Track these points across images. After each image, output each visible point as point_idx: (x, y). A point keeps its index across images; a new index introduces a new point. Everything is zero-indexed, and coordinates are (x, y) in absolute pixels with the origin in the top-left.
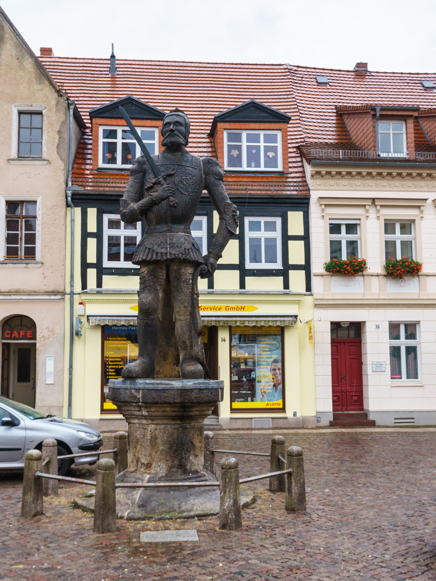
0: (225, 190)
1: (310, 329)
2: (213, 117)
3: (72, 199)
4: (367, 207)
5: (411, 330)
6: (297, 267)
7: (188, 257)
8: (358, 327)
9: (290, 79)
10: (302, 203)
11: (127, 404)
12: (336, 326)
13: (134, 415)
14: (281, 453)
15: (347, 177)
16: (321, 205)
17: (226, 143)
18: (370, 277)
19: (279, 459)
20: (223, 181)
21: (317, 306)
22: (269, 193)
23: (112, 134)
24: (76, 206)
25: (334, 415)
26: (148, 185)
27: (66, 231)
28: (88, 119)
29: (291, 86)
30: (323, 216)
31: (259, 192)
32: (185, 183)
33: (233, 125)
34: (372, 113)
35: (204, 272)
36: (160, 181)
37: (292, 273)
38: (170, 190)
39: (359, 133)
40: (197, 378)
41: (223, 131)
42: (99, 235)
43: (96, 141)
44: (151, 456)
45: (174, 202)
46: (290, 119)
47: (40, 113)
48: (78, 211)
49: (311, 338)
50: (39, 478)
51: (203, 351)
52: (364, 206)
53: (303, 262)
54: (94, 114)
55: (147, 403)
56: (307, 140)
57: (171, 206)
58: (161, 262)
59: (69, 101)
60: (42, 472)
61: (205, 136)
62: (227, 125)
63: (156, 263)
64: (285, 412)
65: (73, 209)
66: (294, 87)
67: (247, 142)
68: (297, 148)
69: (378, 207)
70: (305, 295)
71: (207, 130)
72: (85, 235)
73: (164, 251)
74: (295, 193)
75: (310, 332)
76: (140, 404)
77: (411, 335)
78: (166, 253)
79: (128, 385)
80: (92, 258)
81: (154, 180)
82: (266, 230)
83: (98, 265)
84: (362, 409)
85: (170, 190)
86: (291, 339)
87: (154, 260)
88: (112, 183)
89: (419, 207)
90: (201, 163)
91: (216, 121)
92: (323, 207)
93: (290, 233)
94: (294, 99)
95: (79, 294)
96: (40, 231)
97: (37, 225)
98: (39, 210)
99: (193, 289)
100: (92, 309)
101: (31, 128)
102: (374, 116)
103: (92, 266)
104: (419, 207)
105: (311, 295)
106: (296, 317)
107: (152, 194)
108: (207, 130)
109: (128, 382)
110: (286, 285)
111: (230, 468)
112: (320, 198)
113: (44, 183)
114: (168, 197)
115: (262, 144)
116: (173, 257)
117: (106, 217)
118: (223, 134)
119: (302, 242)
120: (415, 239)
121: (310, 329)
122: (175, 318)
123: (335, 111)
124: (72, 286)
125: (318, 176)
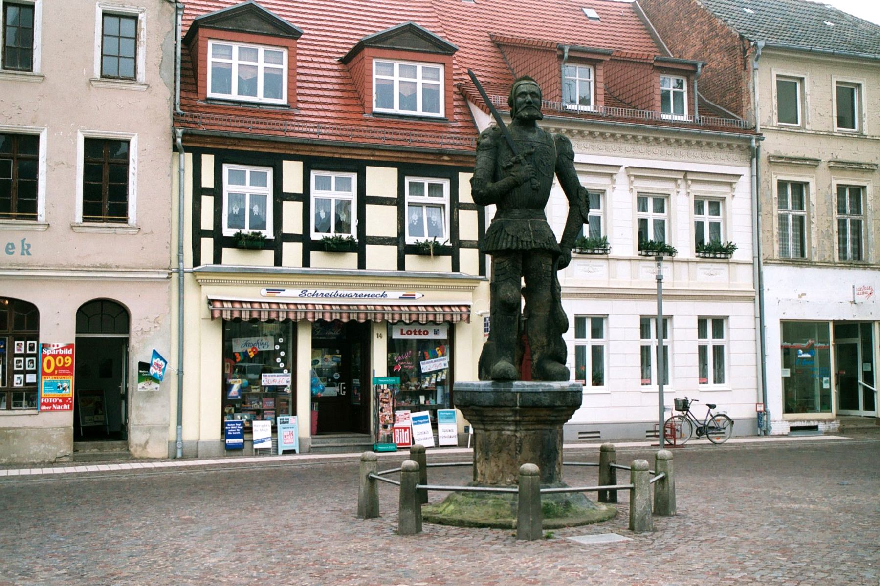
4: (679, 182)
5: (719, 323)
18: (616, 261)
27: (171, 185)
31: (326, 137)
34: (559, 53)
37: (286, 246)
42: (216, 192)
43: (206, 61)
47: (135, 18)
48: (189, 157)
52: (675, 180)
57: (533, 189)
61: (334, 61)
65: (182, 156)
69: (690, 182)
72: (199, 191)
74: (461, 148)
77: (597, 332)
79: (502, 387)
80: (207, 223)
82: (337, 189)
89: (611, 175)
92: (632, 178)
93: (369, 193)
94: (436, 19)
101: (119, 37)
102: (561, 57)
103: (207, 234)
104: (731, 184)
120: (725, 220)
123: (489, 39)
124: (180, 260)
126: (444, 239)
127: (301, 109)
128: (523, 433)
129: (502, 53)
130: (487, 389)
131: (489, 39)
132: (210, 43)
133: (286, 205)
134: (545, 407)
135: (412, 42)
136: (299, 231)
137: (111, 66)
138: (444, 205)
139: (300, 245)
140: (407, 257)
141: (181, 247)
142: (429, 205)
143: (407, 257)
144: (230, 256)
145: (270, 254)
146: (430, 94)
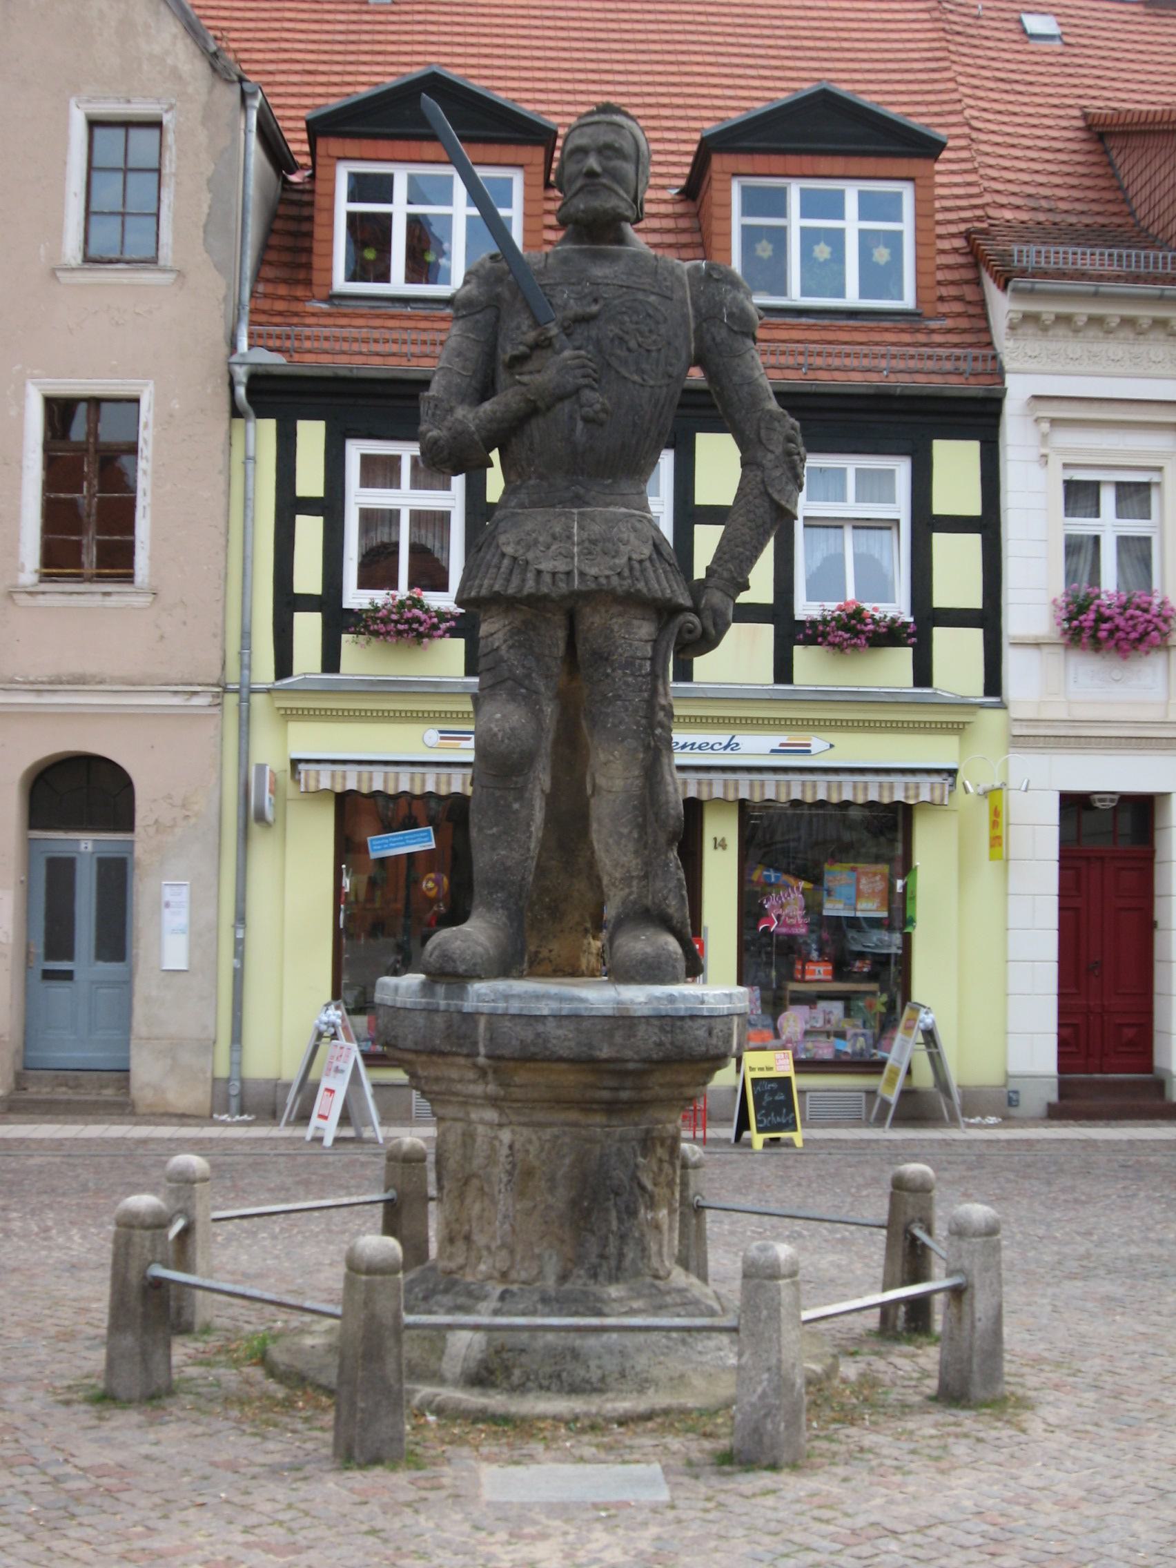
0: (768, 368)
1: (996, 813)
2: (697, 136)
3: (249, 392)
7: (641, 585)
8: (1142, 811)
9: (937, 20)
10: (978, 417)
11: (435, 1058)
12: (1074, 805)
13: (456, 1094)
14: (921, 1220)
15: (1121, 334)
16: (1037, 420)
17: (737, 221)
19: (914, 1239)
20: (755, 340)
21: (1018, 741)
22: (874, 377)
23: (380, 188)
24: (260, 414)
26: (508, 351)
28: (302, 141)
29: (944, 44)
30: (1044, 456)
32: (633, 344)
33: (761, 162)
36: (550, 339)
37: (942, 636)
38: (584, 366)
39: (1157, 195)
41: (729, 182)
42: (330, 506)
43: (331, 210)
45: (598, 407)
46: (942, 146)
47: (157, 124)
48: (268, 428)
49: (996, 841)
50: (159, 1283)
54: (319, 128)
55: (500, 1058)
56: (992, 212)
58: (553, 601)
59: (246, 86)
60: (167, 1267)
62: (742, 162)
63: (536, 602)
65: (251, 425)
66: (952, 48)
67: (804, 215)
68: (967, 235)
70: (982, 706)
71: (676, 176)
72: (290, 505)
73: (561, 566)
75: (995, 824)
76: (481, 1060)
78: (569, 574)
80: (308, 579)
81: (531, 336)
82: (415, 485)
83: (328, 602)
84: (1148, 1067)
85: (584, 366)
86: (931, 847)
87: (530, 596)
88: (376, 341)
90: (686, 278)
91: (709, 147)
92: (1045, 426)
94: (951, 85)
95: (268, 691)
96: (149, 493)
97: (140, 474)
98: (146, 426)
100: (312, 739)
101: (126, 171)
103: (308, 603)
105: (1002, 706)
106: (952, 773)
107: (525, 379)
108: (676, 176)
110: (923, 675)
112: (1036, 397)
113: (167, 341)
114: (577, 391)
115: (852, 224)
116: (593, 586)
117: (355, 450)
118: (729, 190)
120: (1161, 526)
121: (996, 813)
122: (594, 786)
123: (1080, 124)
124: (246, 665)
125: (1030, 329)
126: (899, 607)
129: (1106, 152)
133: (941, 542)
134: (561, 1059)
135: (829, 130)
137: (106, 235)
138: (897, 522)
139: (768, 629)
141: (246, 636)
142: (862, 525)
144: (356, 656)
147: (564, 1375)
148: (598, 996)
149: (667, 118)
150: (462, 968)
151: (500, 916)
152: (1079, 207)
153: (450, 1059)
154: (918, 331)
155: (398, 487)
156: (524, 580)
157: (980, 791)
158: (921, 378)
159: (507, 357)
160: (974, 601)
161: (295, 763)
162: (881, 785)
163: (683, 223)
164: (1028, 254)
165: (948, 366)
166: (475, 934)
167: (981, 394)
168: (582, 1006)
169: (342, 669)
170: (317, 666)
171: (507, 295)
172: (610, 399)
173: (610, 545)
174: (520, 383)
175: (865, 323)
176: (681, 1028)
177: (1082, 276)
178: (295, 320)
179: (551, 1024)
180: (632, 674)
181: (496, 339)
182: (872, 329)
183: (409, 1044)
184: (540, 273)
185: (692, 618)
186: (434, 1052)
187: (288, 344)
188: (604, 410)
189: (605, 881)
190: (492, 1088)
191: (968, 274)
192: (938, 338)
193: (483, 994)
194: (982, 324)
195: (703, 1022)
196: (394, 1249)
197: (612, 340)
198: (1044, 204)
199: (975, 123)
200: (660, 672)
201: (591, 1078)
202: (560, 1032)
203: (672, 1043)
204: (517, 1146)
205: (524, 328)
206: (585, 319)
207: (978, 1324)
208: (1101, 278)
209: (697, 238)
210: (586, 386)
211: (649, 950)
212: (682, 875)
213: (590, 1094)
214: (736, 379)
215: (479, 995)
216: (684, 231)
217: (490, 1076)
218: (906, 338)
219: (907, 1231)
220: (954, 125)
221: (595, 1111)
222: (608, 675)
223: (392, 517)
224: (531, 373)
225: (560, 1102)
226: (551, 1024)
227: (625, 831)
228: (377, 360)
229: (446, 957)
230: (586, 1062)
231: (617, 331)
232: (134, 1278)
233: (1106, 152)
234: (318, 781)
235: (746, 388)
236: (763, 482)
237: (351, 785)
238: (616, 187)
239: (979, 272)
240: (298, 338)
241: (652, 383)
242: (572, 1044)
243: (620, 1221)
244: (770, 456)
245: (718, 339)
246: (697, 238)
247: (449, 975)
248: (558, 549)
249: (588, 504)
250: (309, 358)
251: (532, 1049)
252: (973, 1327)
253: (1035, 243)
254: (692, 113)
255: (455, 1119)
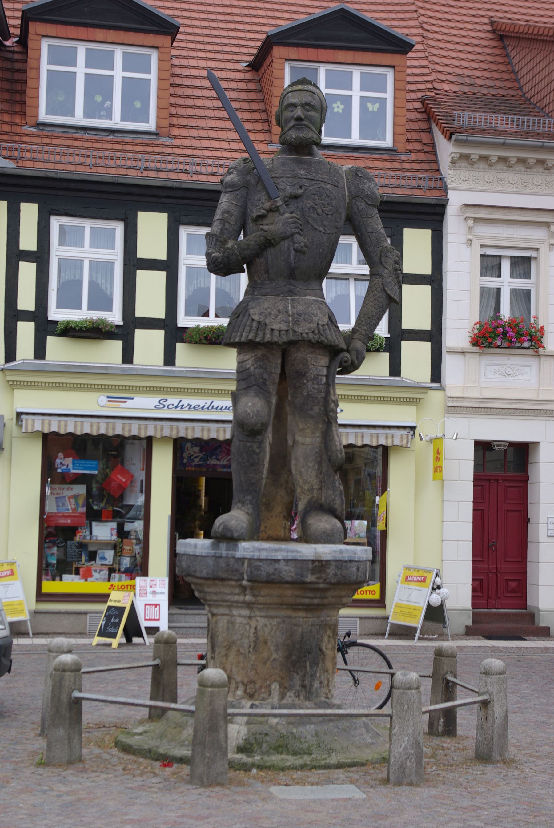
1: (438, 452)
6: (416, 335)
8: (521, 454)
10: (431, 215)
11: (217, 582)
12: (483, 448)
14: (451, 672)
16: (466, 219)
19: (448, 681)
21: (451, 410)
25: (474, 614)
30: (470, 240)
32: (320, 211)
33: (303, 52)
35: (345, 364)
37: (140, 334)
39: (537, 79)
40: (334, 543)
42: (41, 257)
43: (38, 69)
44: (256, 670)
45: (302, 244)
49: (438, 469)
51: (343, 497)
53: (427, 326)
56: (436, 85)
62: (292, 52)
63: (269, 345)
64: (384, 607)
68: (422, 100)
70: (430, 388)
72: (15, 255)
73: (284, 327)
75: (437, 459)
76: (245, 583)
79: (223, 550)
80: (26, 301)
81: (267, 205)
82: (93, 245)
84: (524, 606)
87: (268, 342)
92: (471, 223)
99: (328, 393)
100: (30, 400)
103: (26, 316)
105: (442, 389)
106: (413, 428)
107: (265, 227)
109: (223, 546)
111: (410, 688)
112: (466, 205)
114: (292, 235)
117: (56, 222)
118: (283, 69)
119: (427, 289)
121: (438, 452)
123: (489, 28)
125: (463, 163)
126: (115, 317)
127: (176, 137)
128: (262, 621)
129: (504, 48)
130: (204, 552)
131: (489, 28)
132: (45, 44)
133: (142, 275)
134: (287, 582)
136: (160, 313)
140: (179, 346)
143: (179, 346)
144: (58, 349)
145: (115, 347)
146: (134, 90)
147: (289, 746)
148: (308, 551)
149: (237, 15)
150: (236, 535)
151: (249, 508)
152: (489, 83)
153: (226, 583)
154: (395, 161)
155: (83, 246)
156: (264, 334)
157: (428, 439)
158: (398, 191)
159: (255, 215)
160: (426, 325)
161: (19, 414)
162: (371, 435)
163: (251, 86)
164: (464, 117)
165: (414, 183)
166: (236, 518)
167: (434, 202)
168: (299, 554)
169: (47, 357)
170: (31, 355)
171: (253, 181)
172: (308, 240)
173: (307, 316)
174: (262, 230)
175: (363, 155)
176: (345, 567)
177: (495, 132)
178: (17, 138)
179: (282, 563)
180: (317, 384)
181: (247, 204)
182: (367, 159)
183: (204, 574)
184: (270, 170)
185: (347, 354)
186: (215, 579)
187: (16, 154)
188: (306, 246)
189: (299, 490)
190: (248, 598)
191: (423, 125)
192: (407, 166)
193: (247, 548)
194: (432, 158)
195: (355, 564)
196: (220, 673)
197: (309, 209)
198: (467, 80)
199: (425, 26)
200: (331, 383)
201: (299, 593)
202: (287, 568)
203: (341, 574)
204: (259, 628)
205: (263, 200)
206: (295, 197)
207: (496, 720)
208: (506, 133)
209: (260, 96)
210: (297, 233)
211: (328, 526)
212: (342, 488)
213: (299, 600)
214: (369, 230)
215: (244, 549)
216: (252, 91)
217: (248, 592)
218: (388, 165)
219: (444, 678)
220: (412, 27)
221: (300, 609)
222: (304, 384)
223: (78, 264)
224: (267, 224)
225: (281, 605)
226: (282, 563)
227: (311, 465)
228: (72, 168)
229: (226, 528)
230: (298, 584)
231: (312, 204)
232: (64, 698)
233: (504, 48)
234: (33, 426)
235: (374, 235)
236: (383, 284)
237: (54, 429)
238: (311, 126)
239: (430, 125)
240: (22, 151)
241: (329, 232)
242: (293, 574)
243: (311, 668)
244: (386, 271)
245: (360, 208)
246: (260, 96)
247: (229, 538)
248: (278, 316)
249: (296, 294)
250: (28, 164)
251: (273, 577)
252: (494, 721)
253: (468, 111)
254: (252, 12)
255: (223, 615)
